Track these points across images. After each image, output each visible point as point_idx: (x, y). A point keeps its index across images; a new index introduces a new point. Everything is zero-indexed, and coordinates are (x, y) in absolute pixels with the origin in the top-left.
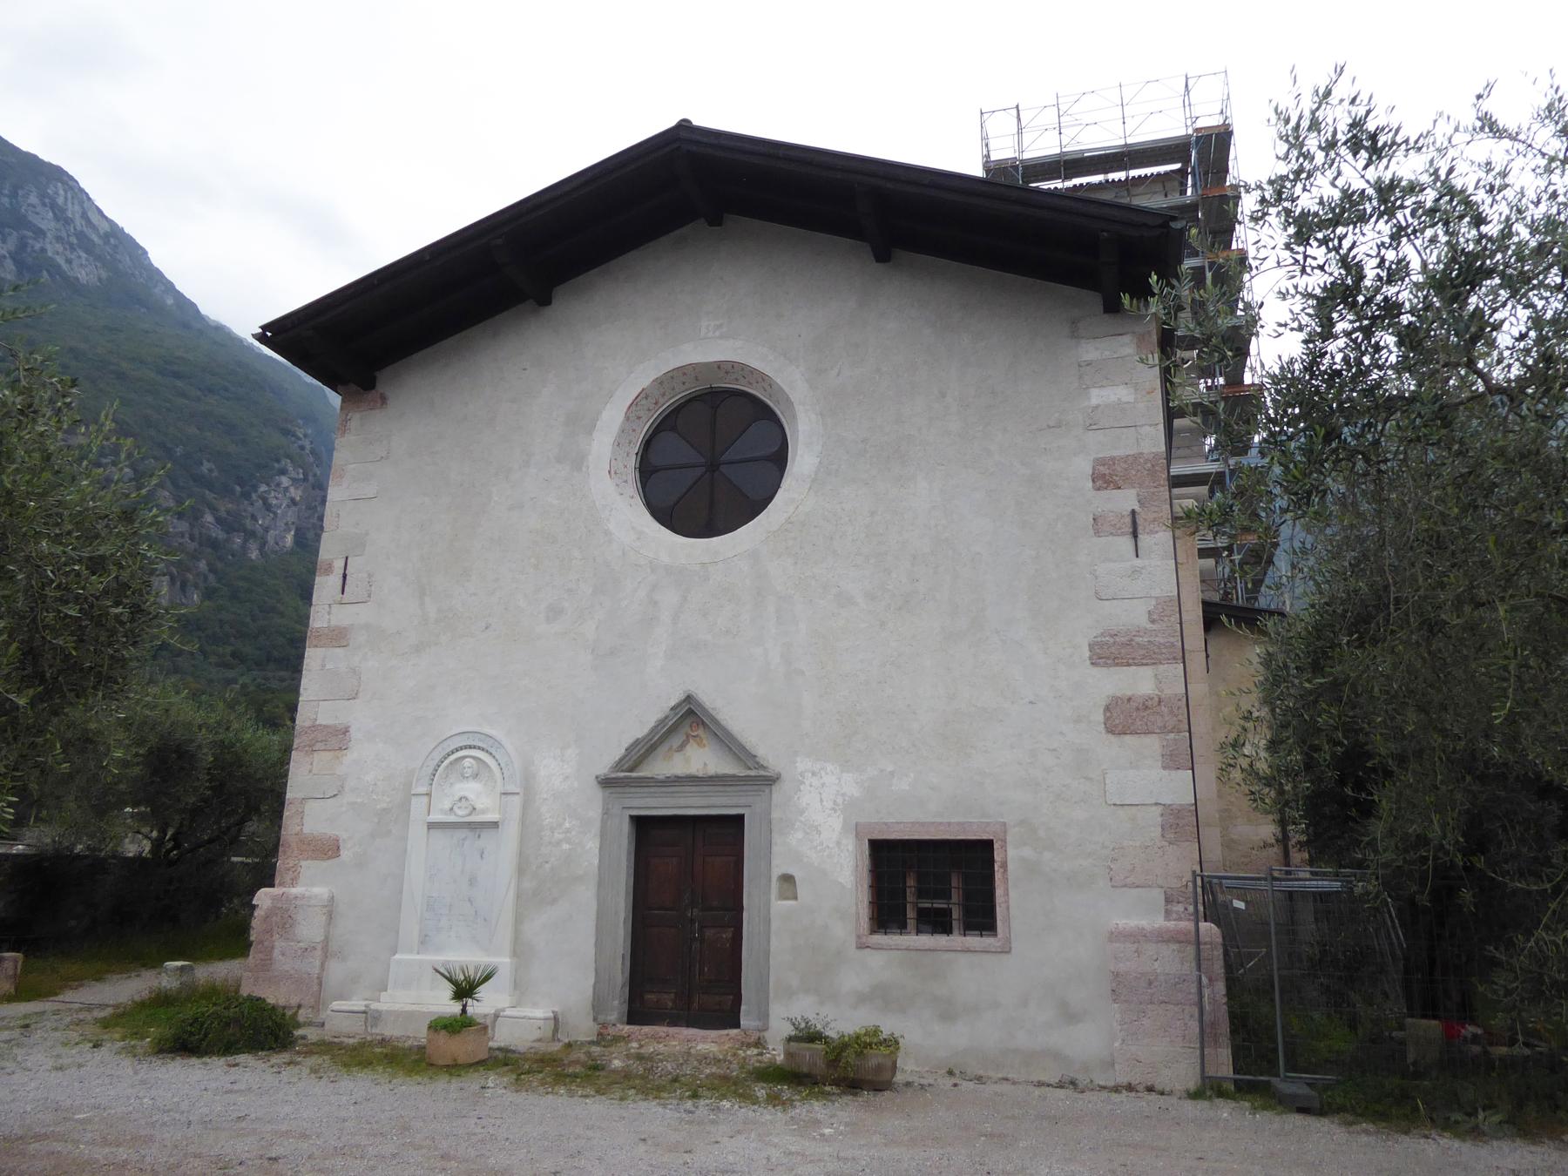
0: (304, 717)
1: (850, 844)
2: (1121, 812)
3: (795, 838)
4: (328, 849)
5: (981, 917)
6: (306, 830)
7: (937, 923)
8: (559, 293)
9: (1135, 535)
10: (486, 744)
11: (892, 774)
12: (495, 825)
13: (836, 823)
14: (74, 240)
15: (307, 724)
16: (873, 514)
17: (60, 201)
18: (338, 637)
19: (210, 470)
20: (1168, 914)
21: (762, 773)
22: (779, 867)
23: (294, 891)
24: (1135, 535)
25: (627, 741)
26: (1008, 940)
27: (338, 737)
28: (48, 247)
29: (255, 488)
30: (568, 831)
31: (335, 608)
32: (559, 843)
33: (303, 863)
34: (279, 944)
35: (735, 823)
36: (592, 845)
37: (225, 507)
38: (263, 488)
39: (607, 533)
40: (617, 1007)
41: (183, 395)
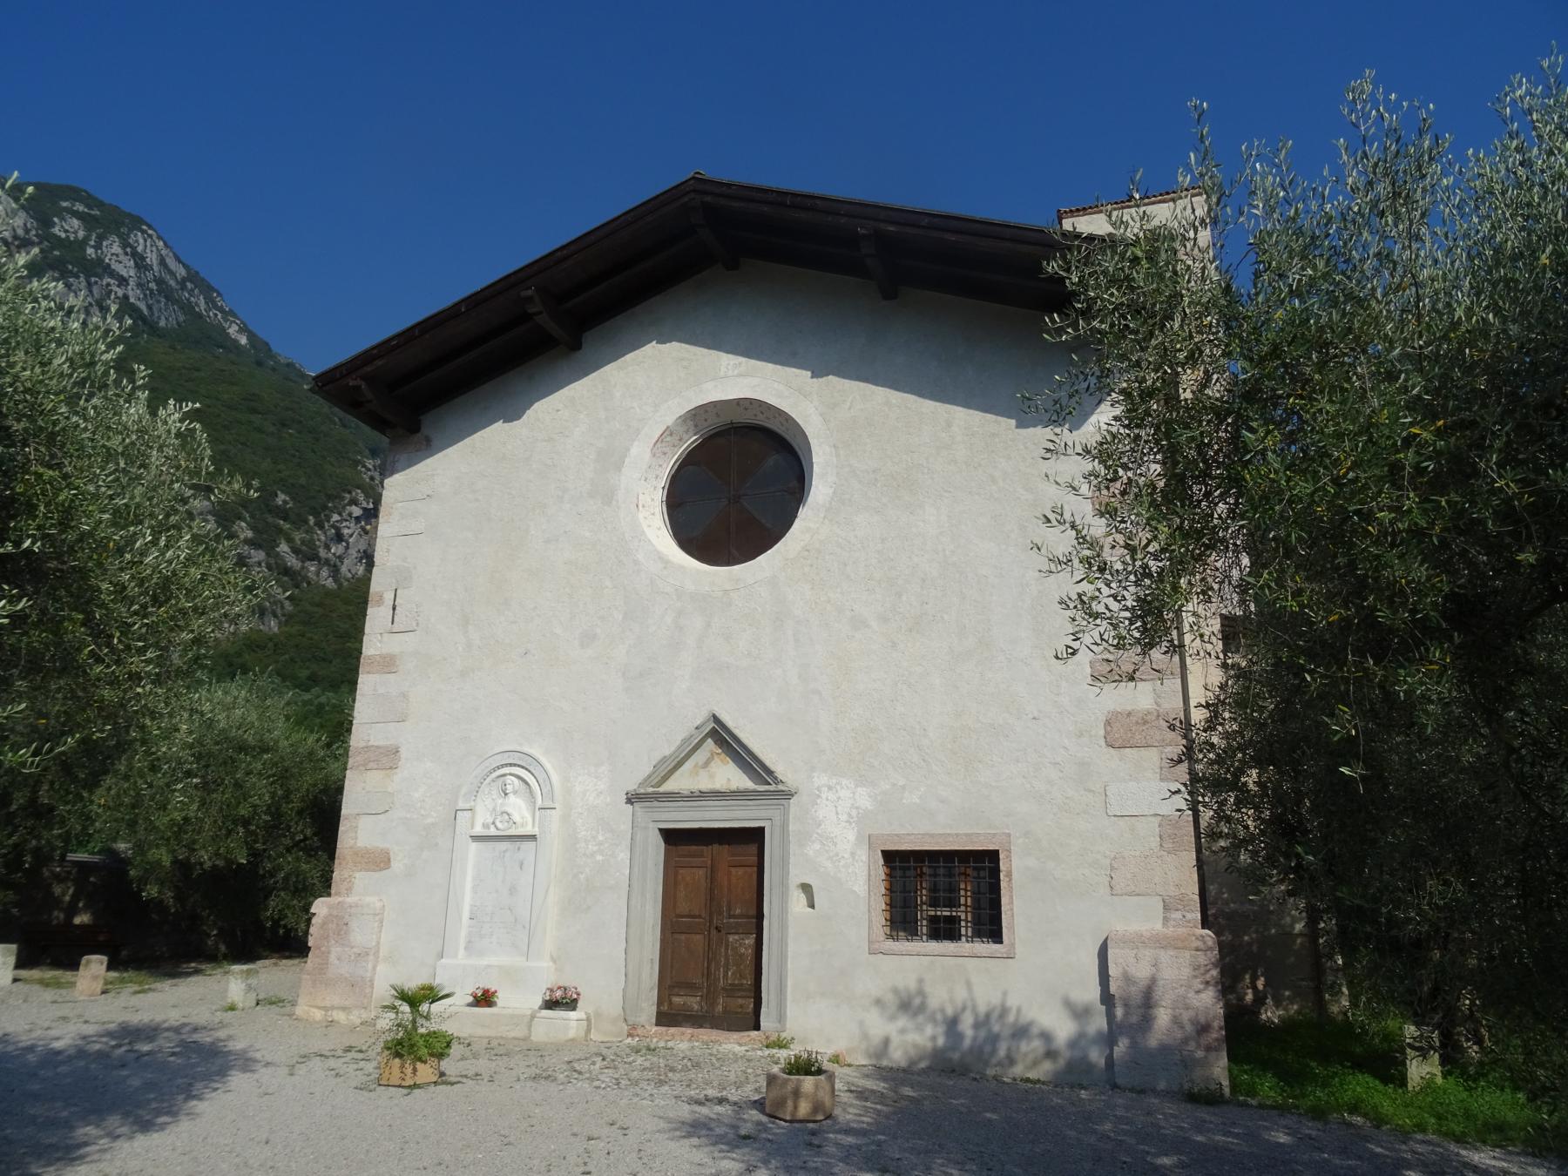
0: (357, 739)
1: (863, 855)
2: (1122, 823)
3: (813, 848)
4: (379, 861)
5: (990, 926)
6: (360, 844)
7: (944, 930)
8: (588, 337)
10: (525, 762)
11: (903, 787)
12: (533, 837)
13: (851, 836)
14: (153, 285)
15: (362, 744)
16: (883, 540)
17: (140, 249)
18: (388, 664)
19: (285, 502)
20: (1166, 920)
21: (780, 787)
22: (797, 876)
23: (349, 900)
25: (657, 756)
26: (1013, 945)
27: (389, 757)
28: (130, 293)
29: (328, 518)
30: (600, 844)
32: (593, 855)
33: (357, 875)
34: (336, 950)
35: (755, 836)
36: (624, 856)
37: (298, 536)
38: (336, 517)
39: (636, 562)
40: (649, 1009)
41: (260, 430)
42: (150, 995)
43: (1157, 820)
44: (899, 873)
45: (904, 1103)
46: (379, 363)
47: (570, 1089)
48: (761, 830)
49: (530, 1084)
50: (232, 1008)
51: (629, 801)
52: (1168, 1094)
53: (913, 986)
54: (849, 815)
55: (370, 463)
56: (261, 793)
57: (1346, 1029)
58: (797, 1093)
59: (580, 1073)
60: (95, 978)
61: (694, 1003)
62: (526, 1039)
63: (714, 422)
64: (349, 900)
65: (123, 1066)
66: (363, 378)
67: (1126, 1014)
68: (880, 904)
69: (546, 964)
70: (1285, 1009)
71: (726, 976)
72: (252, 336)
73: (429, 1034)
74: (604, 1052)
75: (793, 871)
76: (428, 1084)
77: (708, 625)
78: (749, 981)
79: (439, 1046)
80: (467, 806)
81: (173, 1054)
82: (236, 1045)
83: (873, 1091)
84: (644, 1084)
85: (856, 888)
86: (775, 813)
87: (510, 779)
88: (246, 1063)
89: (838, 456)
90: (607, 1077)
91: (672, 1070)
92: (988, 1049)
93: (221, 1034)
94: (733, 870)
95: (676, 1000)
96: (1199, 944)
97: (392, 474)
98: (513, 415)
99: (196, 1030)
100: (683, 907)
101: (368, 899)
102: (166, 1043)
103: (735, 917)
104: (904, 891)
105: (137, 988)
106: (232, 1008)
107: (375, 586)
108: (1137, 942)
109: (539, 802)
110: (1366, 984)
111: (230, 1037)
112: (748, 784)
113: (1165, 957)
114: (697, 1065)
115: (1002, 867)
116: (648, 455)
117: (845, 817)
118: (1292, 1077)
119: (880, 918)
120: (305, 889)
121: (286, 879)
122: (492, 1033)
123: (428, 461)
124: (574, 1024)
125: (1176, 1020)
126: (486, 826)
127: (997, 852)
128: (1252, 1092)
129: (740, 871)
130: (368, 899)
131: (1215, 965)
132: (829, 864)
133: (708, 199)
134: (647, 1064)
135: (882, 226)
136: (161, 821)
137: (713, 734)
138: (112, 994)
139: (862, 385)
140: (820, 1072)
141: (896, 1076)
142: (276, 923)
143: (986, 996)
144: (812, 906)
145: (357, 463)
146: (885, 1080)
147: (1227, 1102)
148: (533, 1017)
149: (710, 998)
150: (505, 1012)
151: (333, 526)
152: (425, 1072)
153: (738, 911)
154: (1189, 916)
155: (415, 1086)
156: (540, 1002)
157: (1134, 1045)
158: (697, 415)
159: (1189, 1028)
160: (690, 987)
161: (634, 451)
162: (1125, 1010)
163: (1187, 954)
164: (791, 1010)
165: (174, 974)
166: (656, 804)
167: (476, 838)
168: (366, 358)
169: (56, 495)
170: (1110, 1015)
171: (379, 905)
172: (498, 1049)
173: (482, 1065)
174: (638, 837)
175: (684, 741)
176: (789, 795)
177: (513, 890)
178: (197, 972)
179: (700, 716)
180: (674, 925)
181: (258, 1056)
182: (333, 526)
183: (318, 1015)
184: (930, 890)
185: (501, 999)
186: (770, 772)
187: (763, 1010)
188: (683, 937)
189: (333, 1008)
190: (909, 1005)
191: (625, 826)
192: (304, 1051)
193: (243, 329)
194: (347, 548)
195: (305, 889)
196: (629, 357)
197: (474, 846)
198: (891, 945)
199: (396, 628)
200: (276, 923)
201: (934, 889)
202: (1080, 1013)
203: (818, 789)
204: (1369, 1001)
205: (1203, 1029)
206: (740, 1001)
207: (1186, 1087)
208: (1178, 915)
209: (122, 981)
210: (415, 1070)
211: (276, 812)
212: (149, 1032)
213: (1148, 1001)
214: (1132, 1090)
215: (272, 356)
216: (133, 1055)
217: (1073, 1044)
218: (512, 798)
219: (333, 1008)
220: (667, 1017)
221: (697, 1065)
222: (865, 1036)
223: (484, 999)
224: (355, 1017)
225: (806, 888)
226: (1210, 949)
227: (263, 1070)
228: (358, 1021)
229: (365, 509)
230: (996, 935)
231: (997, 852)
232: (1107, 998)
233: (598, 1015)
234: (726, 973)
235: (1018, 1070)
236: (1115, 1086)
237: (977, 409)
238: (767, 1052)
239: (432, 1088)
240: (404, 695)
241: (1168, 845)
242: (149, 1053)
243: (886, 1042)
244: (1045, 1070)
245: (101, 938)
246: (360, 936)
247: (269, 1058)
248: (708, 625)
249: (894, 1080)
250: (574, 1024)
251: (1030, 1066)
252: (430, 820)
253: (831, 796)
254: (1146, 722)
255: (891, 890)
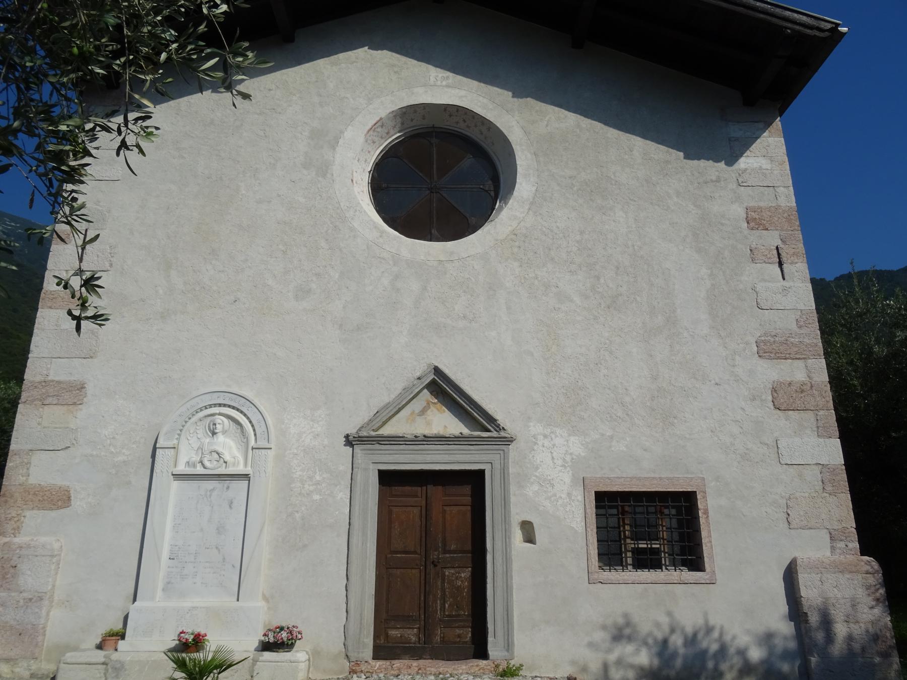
0: (31, 374)
1: (578, 495)
2: (791, 470)
3: (531, 490)
6: (32, 480)
7: (647, 561)
11: (611, 437)
12: (246, 477)
13: (567, 478)
15: (39, 378)
20: (833, 548)
21: (503, 434)
22: (517, 517)
23: (17, 540)
24: (781, 264)
27: (73, 393)
30: (318, 483)
33: (28, 513)
36: (343, 495)
48: (481, 473)
54: (564, 460)
61: (412, 634)
75: (514, 510)
77: (425, 289)
85: (574, 525)
86: (496, 458)
87: (219, 419)
94: (445, 508)
95: (393, 633)
96: (868, 568)
101: (43, 539)
103: (450, 552)
108: (818, 567)
112: (466, 431)
115: (700, 506)
116: (361, 139)
117: (560, 462)
129: (455, 509)
130: (43, 539)
131: (882, 586)
132: (547, 503)
143: (690, 620)
149: (426, 631)
153: (453, 547)
154: (851, 545)
156: (256, 644)
158: (408, 113)
160: (405, 620)
161: (348, 134)
163: (860, 577)
164: (519, 638)
166: (377, 446)
167: (178, 477)
176: (509, 441)
186: (492, 420)
188: (398, 572)
190: (621, 633)
191: (345, 467)
196: (341, 56)
197: (176, 484)
198: (608, 575)
201: (634, 525)
206: (458, 631)
208: (841, 545)
218: (221, 438)
226: (877, 572)
241: (829, 488)
248: (425, 289)
253: (546, 443)
254: (802, 391)
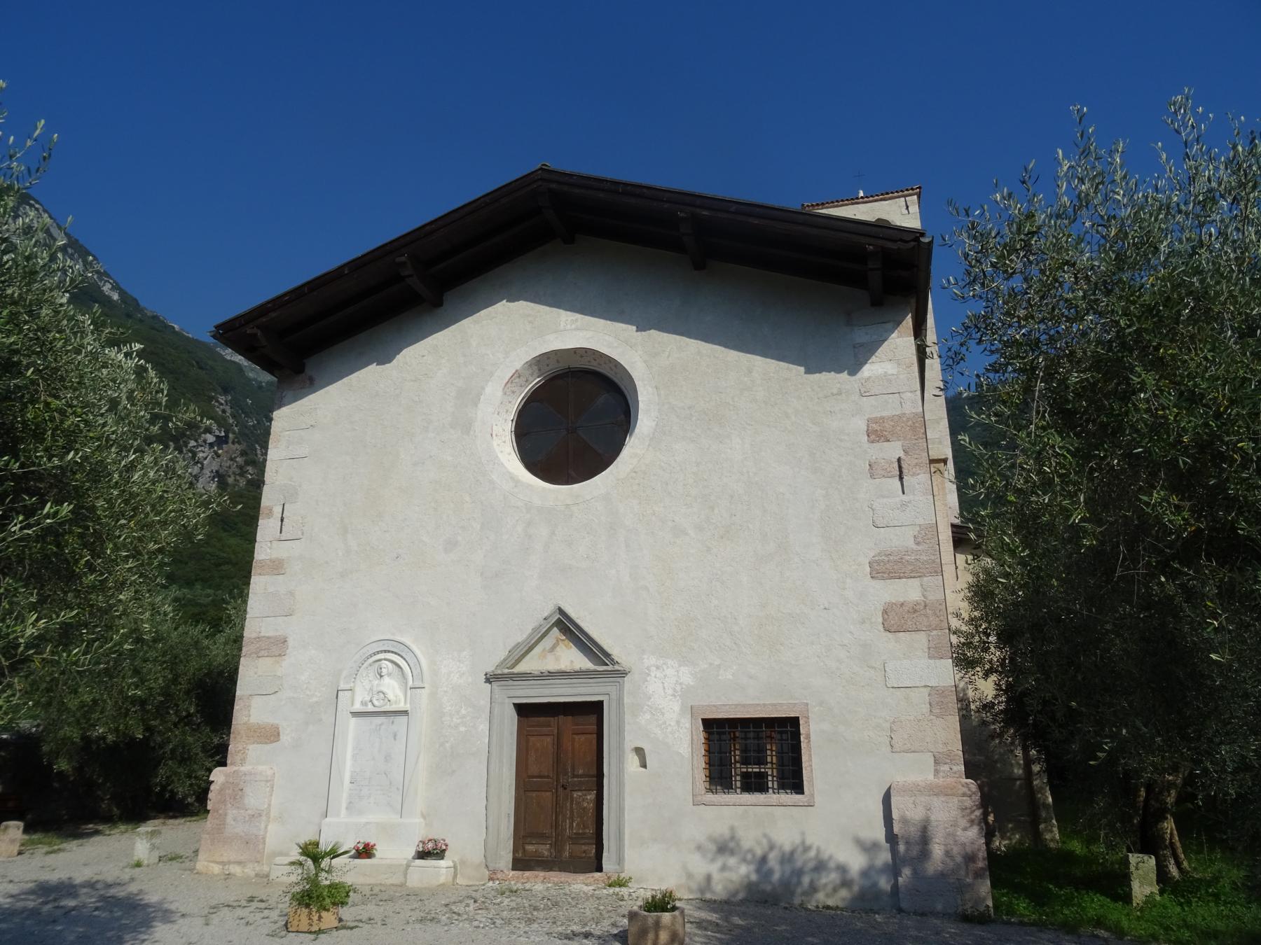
2: (898, 693)
3: (644, 718)
4: (270, 735)
5: (793, 780)
6: (253, 720)
7: (755, 784)
9: (901, 478)
10: (396, 649)
11: (719, 666)
12: (405, 713)
13: (676, 707)
15: (254, 635)
18: (277, 567)
20: (937, 772)
21: (617, 667)
22: (631, 741)
23: (242, 769)
24: (901, 478)
25: (511, 644)
26: (812, 795)
27: (278, 646)
29: (186, 444)
30: (463, 717)
31: (275, 544)
32: (456, 727)
33: (251, 747)
34: (232, 813)
35: (595, 709)
36: (483, 727)
38: (193, 443)
42: (61, 854)
43: (926, 691)
44: (716, 737)
45: (737, 932)
46: (273, 315)
47: (454, 930)
48: (600, 703)
49: (418, 926)
50: (138, 865)
51: (488, 681)
52: (944, 915)
53: (727, 833)
54: (675, 690)
55: (222, 399)
56: (157, 678)
57: (1066, 857)
58: (657, 925)
59: (459, 915)
60: (12, 841)
61: (545, 850)
62: (402, 885)
63: (554, 367)
64: (242, 769)
65: (54, 921)
66: (258, 327)
67: (907, 850)
68: (701, 763)
69: (418, 820)
70: (1010, 839)
71: (571, 827)
72: (122, 293)
73: (330, 886)
74: (474, 894)
76: (331, 929)
77: (553, 533)
78: (591, 830)
79: (339, 895)
80: (348, 687)
81: (97, 909)
82: (153, 898)
83: (710, 922)
84: (516, 923)
88: (167, 916)
89: (659, 395)
90: (482, 916)
91: (536, 909)
92: (795, 880)
93: (133, 888)
94: (576, 737)
95: (530, 848)
96: (965, 790)
97: (280, 407)
98: (385, 359)
99: (109, 886)
100: (534, 770)
101: (260, 768)
102: (88, 899)
103: (578, 776)
104: (720, 752)
105: (46, 848)
106: (138, 865)
107: (265, 501)
108: (914, 790)
109: (410, 683)
110: (1104, 821)
111: (141, 891)
113: (937, 802)
114: (556, 904)
116: (500, 394)
117: (670, 692)
118: (1039, 899)
119: (701, 775)
120: (190, 758)
121: (173, 751)
122: (372, 881)
123: (311, 397)
124: (444, 871)
125: (948, 853)
126: (364, 703)
127: (797, 719)
128: (1011, 912)
129: (583, 738)
130: (260, 768)
133: (554, 186)
134: (513, 905)
135: (698, 210)
136: (72, 703)
137: (559, 623)
138: (26, 855)
139: (678, 337)
140: (674, 908)
141: (724, 906)
142: (164, 788)
144: (644, 765)
145: (212, 398)
146: (714, 911)
147: (993, 921)
148: (408, 866)
149: (557, 845)
150: (384, 862)
151: (190, 451)
152: (329, 919)
153: (581, 772)
154: (955, 768)
155: (320, 932)
157: (915, 873)
158: (541, 361)
159: (959, 859)
160: (541, 837)
161: (488, 390)
162: (904, 846)
163: (956, 800)
164: (629, 853)
165: (77, 835)
167: (356, 714)
168: (262, 310)
169: (62, 422)
170: (894, 851)
171: (269, 773)
172: (379, 895)
173: (371, 910)
174: (496, 711)
175: (535, 630)
176: (623, 674)
177: (387, 758)
178: (97, 832)
179: (548, 609)
180: (527, 784)
181: (173, 907)
182: (190, 451)
183: (216, 869)
184: (742, 751)
185: (379, 852)
186: (607, 655)
187: (605, 854)
188: (534, 794)
189: (229, 863)
190: (724, 848)
191: (484, 702)
192: (214, 902)
193: (116, 287)
194: (202, 468)
195: (190, 758)
196: (483, 313)
197: (353, 721)
198: (711, 797)
199: (284, 536)
200: (164, 788)
201: (745, 750)
202: (869, 848)
203: (648, 668)
204: (1106, 835)
205: (970, 858)
206: (584, 848)
207: (960, 909)
208: (946, 768)
209: (33, 843)
210: (320, 917)
211: (166, 693)
212: (67, 889)
213: (924, 838)
214: (915, 913)
215: (141, 310)
216: (59, 912)
217: (865, 873)
218: (386, 680)
219: (229, 863)
220: (522, 863)
221: (556, 904)
222: (690, 876)
223: (365, 852)
224: (250, 871)
225: (639, 751)
227: (181, 921)
228: (252, 874)
229: (217, 437)
230: (798, 788)
231: (797, 719)
232: (891, 838)
233: (463, 862)
234: (571, 824)
235: (821, 898)
236: (900, 910)
237: (772, 358)
238: (611, 890)
239: (335, 933)
240: (291, 593)
241: (936, 711)
242: (74, 909)
243: (709, 878)
244: (841, 898)
245: (10, 804)
246: (253, 800)
247: (183, 909)
248: (553, 533)
249: (722, 911)
250: (444, 871)
251: (829, 896)
252: (315, 699)
254: (915, 611)
255: (709, 751)
